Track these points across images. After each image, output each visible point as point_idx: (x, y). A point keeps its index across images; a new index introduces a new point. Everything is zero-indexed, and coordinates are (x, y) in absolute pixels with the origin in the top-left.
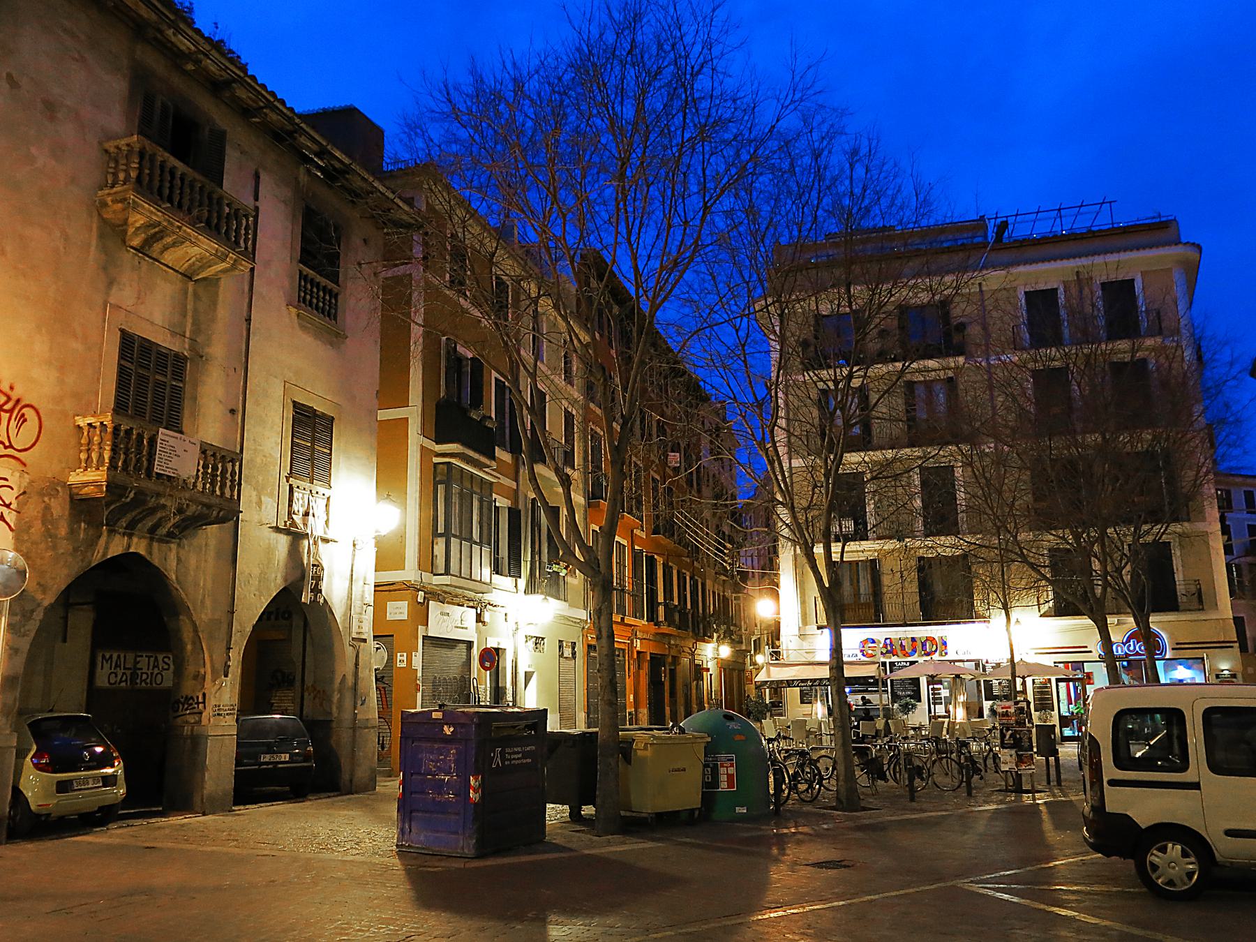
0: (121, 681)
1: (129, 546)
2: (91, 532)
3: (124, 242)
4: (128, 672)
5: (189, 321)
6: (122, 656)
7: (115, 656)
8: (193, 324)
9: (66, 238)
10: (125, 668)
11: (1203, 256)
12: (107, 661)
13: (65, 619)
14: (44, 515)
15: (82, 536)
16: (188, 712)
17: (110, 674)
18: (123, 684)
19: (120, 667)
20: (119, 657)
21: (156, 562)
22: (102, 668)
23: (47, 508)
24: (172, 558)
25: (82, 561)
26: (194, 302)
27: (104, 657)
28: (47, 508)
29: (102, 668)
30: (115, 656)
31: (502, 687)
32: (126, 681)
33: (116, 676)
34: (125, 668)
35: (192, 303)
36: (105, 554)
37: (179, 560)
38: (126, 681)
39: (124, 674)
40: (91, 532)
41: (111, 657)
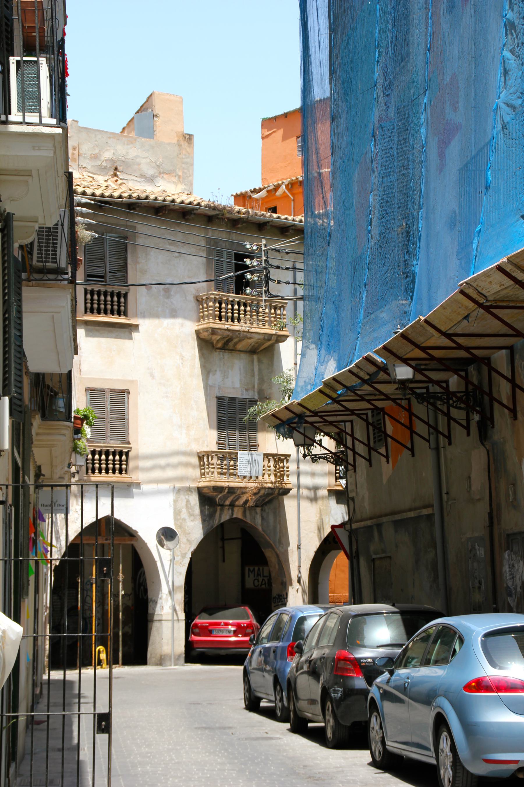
0: (262, 584)
1: (232, 514)
2: (211, 510)
3: (213, 346)
4: (266, 579)
5: (256, 377)
6: (261, 568)
7: (256, 568)
8: (259, 379)
9: (182, 357)
10: (264, 576)
11: (356, 504)
12: (252, 572)
13: (223, 547)
14: (186, 505)
15: (207, 513)
16: (280, 603)
17: (255, 580)
18: (263, 586)
19: (260, 575)
20: (259, 569)
21: (248, 521)
22: (249, 577)
23: (188, 501)
24: (259, 520)
25: (208, 525)
26: (259, 365)
27: (249, 570)
28: (188, 501)
29: (249, 577)
30: (256, 568)
31: (150, 614)
32: (265, 584)
33: (258, 581)
34: (264, 576)
35: (257, 366)
36: (220, 520)
37: (263, 518)
38: (265, 584)
39: (263, 580)
40: (211, 510)
41: (254, 569)
